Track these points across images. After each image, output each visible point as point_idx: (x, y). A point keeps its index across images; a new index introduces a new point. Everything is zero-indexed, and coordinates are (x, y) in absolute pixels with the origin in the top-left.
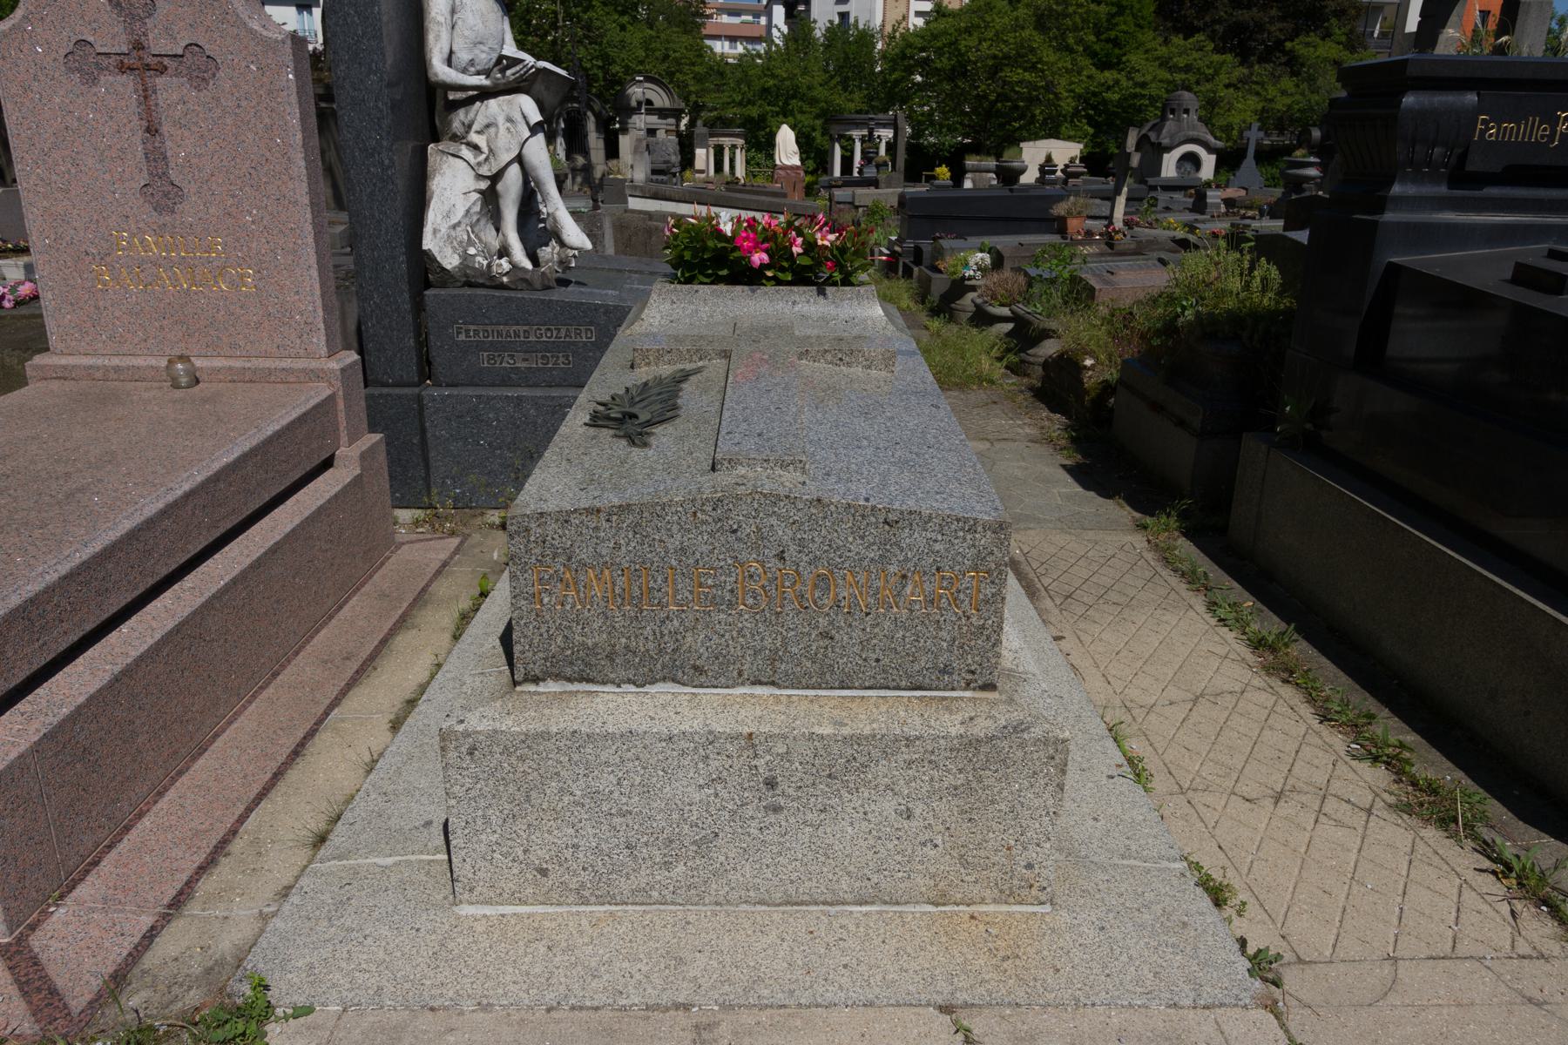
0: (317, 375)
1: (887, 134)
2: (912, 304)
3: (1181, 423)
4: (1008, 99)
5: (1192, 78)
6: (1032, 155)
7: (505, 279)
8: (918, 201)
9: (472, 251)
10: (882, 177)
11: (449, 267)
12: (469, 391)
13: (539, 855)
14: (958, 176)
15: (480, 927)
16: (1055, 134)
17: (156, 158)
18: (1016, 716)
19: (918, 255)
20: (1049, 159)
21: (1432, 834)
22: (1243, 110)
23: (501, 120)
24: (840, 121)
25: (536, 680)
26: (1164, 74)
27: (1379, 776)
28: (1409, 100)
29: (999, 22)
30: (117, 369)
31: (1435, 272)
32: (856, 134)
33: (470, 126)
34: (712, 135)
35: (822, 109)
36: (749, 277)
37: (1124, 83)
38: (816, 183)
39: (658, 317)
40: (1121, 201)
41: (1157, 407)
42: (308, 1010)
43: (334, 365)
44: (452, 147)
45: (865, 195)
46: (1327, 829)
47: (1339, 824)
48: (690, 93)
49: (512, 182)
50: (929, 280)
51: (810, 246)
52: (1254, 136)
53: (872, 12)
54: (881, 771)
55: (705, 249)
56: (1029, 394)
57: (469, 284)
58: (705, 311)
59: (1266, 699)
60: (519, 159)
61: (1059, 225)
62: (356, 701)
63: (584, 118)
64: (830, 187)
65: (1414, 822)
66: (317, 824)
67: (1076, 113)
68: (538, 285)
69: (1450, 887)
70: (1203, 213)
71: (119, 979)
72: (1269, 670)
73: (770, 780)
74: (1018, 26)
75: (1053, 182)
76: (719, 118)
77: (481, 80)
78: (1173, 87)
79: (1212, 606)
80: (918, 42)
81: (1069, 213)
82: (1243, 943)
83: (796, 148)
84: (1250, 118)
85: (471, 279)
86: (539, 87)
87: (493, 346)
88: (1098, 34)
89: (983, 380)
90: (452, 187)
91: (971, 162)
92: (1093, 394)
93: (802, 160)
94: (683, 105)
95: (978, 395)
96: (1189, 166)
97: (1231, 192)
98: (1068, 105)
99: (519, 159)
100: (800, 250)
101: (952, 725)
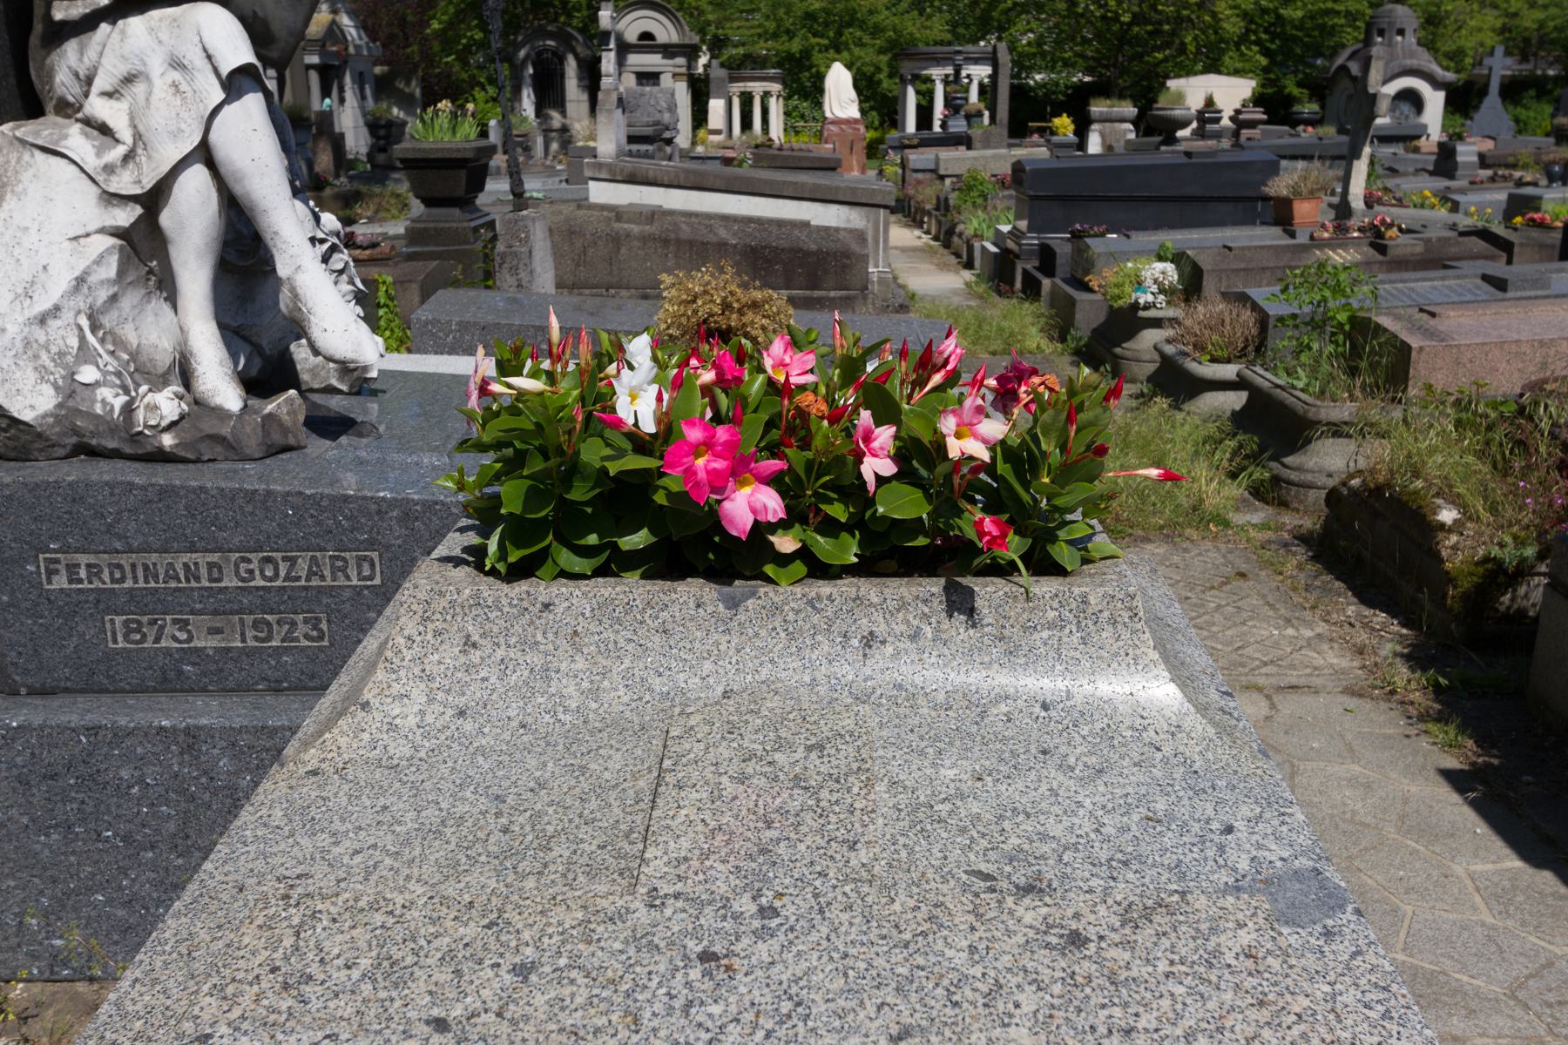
1: (981, 72)
2: (1044, 343)
4: (1148, 21)
6: (1193, 91)
7: (168, 440)
8: (1043, 174)
9: (88, 374)
10: (976, 133)
11: (27, 416)
14: (1083, 125)
16: (1214, 67)
19: (1047, 258)
20: (1210, 102)
23: (156, 65)
24: (911, 56)
32: (937, 73)
33: (89, 81)
34: (733, 79)
35: (890, 41)
38: (881, 141)
39: (418, 694)
45: (954, 159)
48: (708, 23)
49: (192, 215)
50: (1072, 303)
51: (919, 457)
52: (1501, 66)
55: (573, 470)
56: (1301, 553)
60: (204, 153)
61: (1281, 213)
63: (562, 60)
64: (902, 147)
67: (1243, 39)
68: (252, 444)
70: (1451, 177)
75: (1217, 135)
76: (747, 56)
81: (1297, 193)
83: (853, 94)
84: (1490, 39)
89: (1199, 517)
91: (1097, 108)
92: (1465, 584)
93: (862, 111)
94: (696, 39)
95: (1207, 556)
96: (1406, 108)
98: (1233, 27)
99: (204, 153)
100: (887, 468)
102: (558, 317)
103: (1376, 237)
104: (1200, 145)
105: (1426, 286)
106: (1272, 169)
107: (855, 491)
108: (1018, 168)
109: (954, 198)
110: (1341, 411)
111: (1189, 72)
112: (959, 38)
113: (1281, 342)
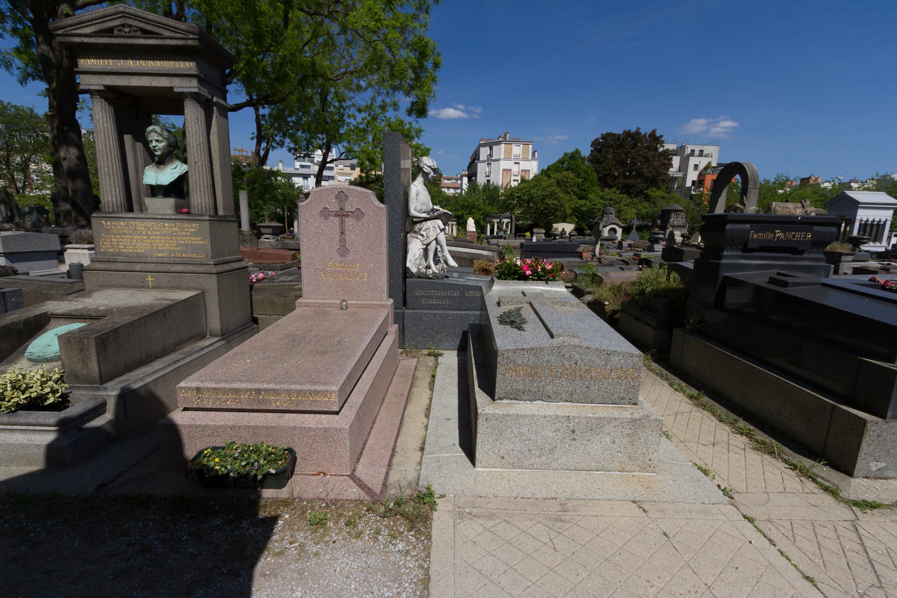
0: (384, 306)
1: (506, 221)
3: (647, 324)
5: (612, 202)
6: (559, 227)
12: (418, 311)
13: (502, 452)
15: (485, 474)
16: (564, 221)
17: (343, 241)
18: (646, 413)
20: (563, 230)
21: (766, 456)
22: (631, 213)
25: (501, 399)
26: (602, 201)
27: (744, 439)
28: (728, 226)
29: (544, 184)
30: (323, 304)
31: (741, 279)
32: (495, 221)
36: (524, 278)
37: (588, 204)
40: (598, 247)
41: (637, 319)
42: (445, 496)
43: (389, 303)
44: (415, 235)
46: (732, 454)
47: (736, 453)
52: (636, 222)
53: (498, 179)
54: (607, 428)
57: (419, 277)
58: (511, 288)
59: (698, 414)
61: (580, 255)
62: (410, 408)
65: (760, 453)
66: (418, 444)
67: (572, 214)
69: (778, 472)
71: (385, 485)
72: (697, 405)
73: (572, 431)
74: (550, 186)
77: (425, 215)
78: (605, 206)
79: (671, 385)
80: (517, 191)
82: (719, 486)
84: (633, 216)
85: (419, 276)
86: (443, 217)
87: (427, 297)
88: (578, 188)
90: (415, 248)
91: (535, 230)
96: (612, 232)
97: (629, 242)
98: (569, 211)
99: (436, 239)
101: (627, 415)
102: (81, 330)
103: (599, 260)
104: (561, 240)
105: (607, 269)
106: (579, 246)
107: (537, 272)
108: (522, 245)
109: (503, 251)
110: (589, 290)
111: (558, 222)
112: (501, 212)
113: (580, 278)
